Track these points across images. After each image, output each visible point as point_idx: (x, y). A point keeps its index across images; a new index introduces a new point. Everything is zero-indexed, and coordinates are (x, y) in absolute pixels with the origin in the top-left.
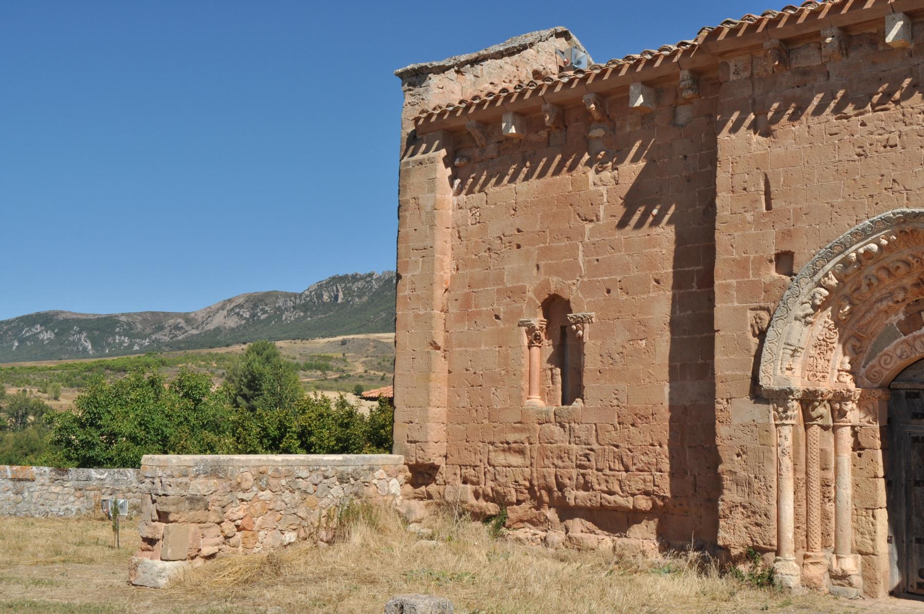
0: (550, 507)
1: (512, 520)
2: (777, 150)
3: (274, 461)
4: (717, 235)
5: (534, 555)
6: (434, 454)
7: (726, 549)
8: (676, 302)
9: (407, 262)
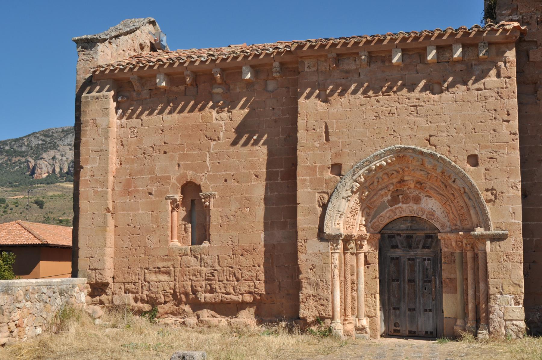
0: (186, 304)
1: (161, 313)
2: (332, 111)
3: (33, 283)
4: (298, 153)
5: (177, 332)
6: (108, 277)
7: (304, 319)
8: (267, 188)
9: (88, 159)
